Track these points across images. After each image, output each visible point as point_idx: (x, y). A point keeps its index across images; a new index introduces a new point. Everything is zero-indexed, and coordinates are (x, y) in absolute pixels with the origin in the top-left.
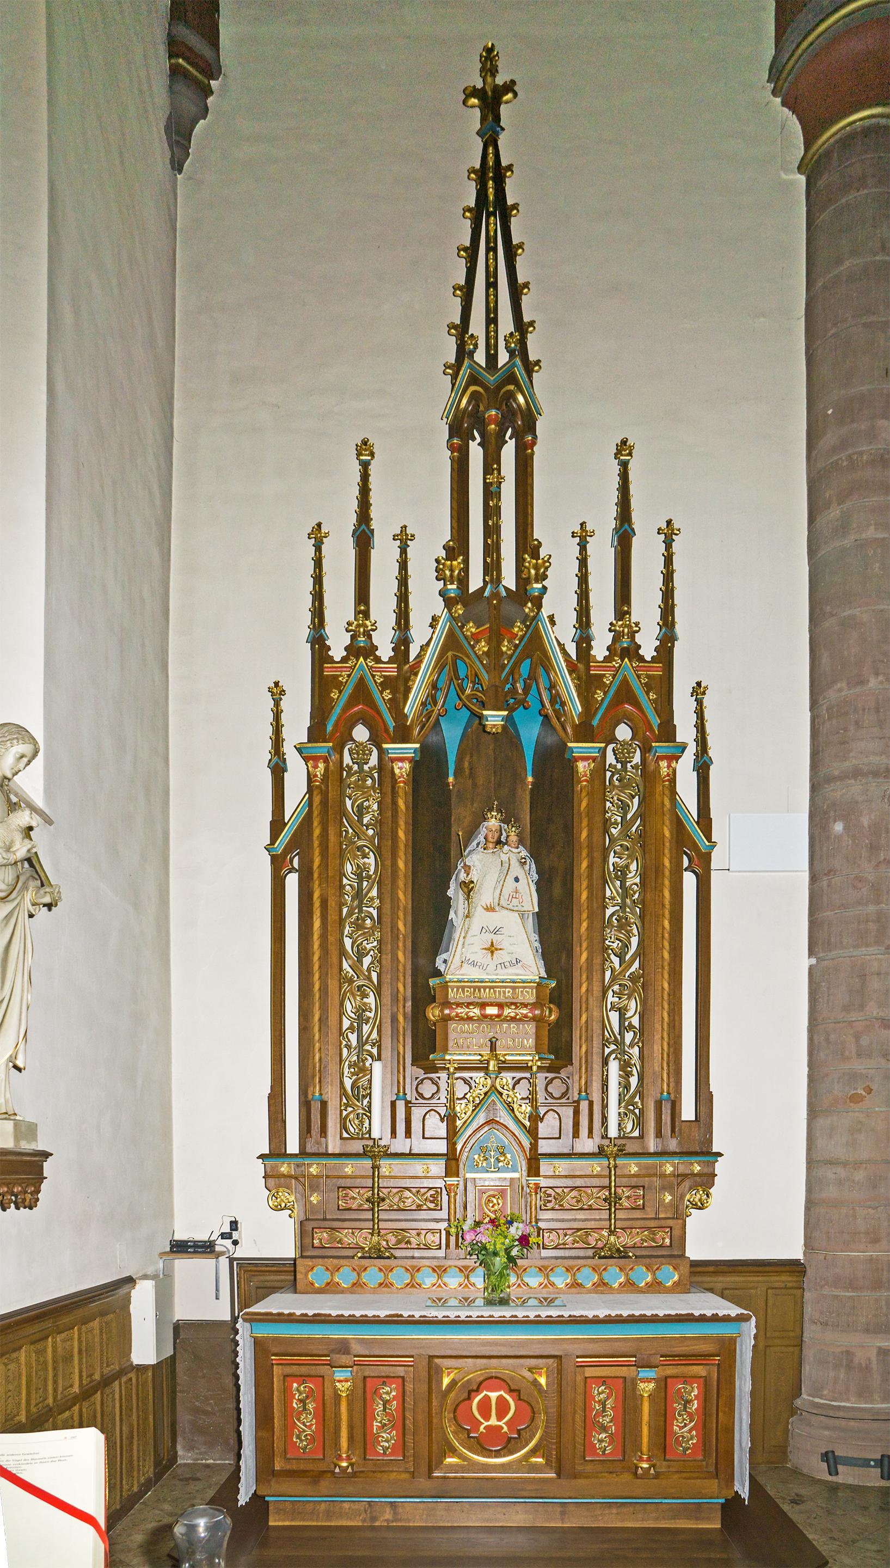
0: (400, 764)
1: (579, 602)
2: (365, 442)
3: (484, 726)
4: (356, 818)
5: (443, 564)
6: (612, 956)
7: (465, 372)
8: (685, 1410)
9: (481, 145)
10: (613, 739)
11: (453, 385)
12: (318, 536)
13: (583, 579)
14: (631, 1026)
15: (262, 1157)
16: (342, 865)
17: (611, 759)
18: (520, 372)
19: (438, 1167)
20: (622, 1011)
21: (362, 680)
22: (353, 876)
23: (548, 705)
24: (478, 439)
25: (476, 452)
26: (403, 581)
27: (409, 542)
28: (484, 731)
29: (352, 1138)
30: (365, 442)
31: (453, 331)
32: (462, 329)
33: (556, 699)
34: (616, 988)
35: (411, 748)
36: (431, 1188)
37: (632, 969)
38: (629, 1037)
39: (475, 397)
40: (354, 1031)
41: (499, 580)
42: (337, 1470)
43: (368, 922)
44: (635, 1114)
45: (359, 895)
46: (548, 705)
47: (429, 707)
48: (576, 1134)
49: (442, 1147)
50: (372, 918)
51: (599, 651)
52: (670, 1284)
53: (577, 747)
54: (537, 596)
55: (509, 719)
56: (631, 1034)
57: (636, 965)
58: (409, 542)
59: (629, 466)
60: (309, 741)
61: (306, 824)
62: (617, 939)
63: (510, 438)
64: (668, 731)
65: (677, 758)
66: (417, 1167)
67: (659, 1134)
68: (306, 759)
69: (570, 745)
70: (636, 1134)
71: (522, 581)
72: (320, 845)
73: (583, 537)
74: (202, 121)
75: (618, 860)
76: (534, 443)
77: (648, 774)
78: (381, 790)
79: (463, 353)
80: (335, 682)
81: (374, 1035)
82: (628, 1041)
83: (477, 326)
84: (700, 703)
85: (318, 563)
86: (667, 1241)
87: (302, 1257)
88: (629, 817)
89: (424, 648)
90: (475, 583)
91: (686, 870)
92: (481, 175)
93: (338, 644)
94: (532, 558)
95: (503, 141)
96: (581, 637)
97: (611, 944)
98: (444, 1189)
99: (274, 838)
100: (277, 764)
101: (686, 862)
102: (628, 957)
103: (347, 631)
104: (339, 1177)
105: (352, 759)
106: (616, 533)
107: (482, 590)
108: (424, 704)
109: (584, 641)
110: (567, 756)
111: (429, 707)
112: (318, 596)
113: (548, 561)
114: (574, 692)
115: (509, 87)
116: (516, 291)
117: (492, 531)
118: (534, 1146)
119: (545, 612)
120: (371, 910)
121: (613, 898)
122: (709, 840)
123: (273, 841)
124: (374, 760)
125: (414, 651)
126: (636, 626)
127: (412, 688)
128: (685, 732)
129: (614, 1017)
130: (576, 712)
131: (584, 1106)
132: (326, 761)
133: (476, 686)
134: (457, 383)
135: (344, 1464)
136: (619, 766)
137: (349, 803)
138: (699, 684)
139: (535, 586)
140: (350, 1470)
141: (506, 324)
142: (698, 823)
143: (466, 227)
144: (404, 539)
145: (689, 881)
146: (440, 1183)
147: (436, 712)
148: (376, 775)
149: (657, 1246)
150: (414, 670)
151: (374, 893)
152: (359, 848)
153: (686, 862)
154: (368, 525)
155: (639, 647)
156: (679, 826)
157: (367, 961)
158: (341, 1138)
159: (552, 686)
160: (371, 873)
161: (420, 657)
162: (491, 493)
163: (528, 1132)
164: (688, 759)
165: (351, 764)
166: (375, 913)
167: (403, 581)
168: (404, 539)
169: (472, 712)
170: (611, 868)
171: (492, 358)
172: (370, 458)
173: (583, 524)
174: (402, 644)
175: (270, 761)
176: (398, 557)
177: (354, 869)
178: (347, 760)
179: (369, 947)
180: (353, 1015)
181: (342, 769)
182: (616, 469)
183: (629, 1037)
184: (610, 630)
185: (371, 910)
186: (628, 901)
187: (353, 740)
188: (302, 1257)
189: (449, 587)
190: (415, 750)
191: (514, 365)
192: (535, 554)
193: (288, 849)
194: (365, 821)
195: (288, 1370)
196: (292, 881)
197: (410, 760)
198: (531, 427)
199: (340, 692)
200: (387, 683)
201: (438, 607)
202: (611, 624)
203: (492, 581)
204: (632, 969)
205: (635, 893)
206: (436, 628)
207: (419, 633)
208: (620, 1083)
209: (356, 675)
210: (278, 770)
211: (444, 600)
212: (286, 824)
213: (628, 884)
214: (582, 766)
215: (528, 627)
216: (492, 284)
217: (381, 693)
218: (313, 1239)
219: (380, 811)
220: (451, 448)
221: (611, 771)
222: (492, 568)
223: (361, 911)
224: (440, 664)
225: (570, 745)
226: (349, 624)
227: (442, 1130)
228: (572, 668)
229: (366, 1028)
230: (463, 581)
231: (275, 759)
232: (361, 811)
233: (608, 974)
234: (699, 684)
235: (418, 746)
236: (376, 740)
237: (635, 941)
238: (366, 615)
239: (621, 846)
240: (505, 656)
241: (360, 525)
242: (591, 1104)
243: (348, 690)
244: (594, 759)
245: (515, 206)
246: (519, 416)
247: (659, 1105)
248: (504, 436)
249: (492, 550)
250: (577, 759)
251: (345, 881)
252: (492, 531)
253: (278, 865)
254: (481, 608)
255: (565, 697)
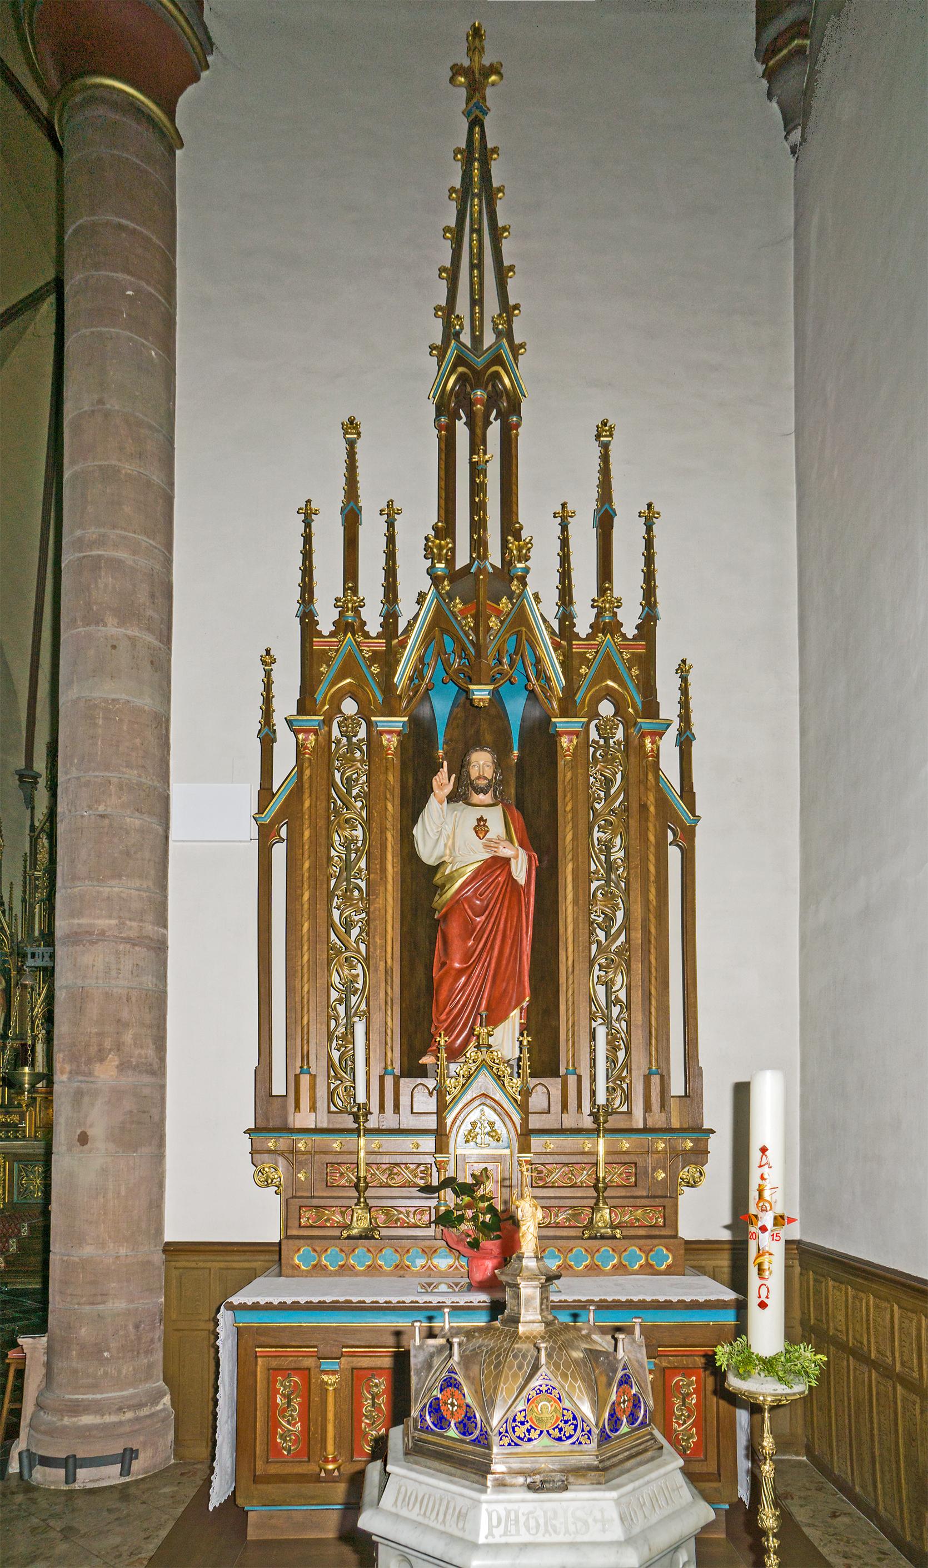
0: (388, 737)
1: (562, 581)
2: (351, 421)
3: (472, 700)
4: (345, 790)
5: (433, 542)
6: (598, 931)
7: (451, 353)
8: (684, 1404)
9: (466, 126)
10: (596, 715)
11: (440, 367)
12: (308, 515)
13: (565, 558)
14: (618, 1000)
15: (248, 1131)
16: (329, 837)
17: (594, 735)
18: (506, 353)
19: (428, 1143)
20: (608, 985)
21: (350, 655)
22: (342, 848)
23: (532, 678)
24: (464, 419)
25: (462, 432)
26: (391, 555)
27: (396, 516)
28: (473, 706)
29: (341, 1112)
30: (351, 421)
31: (448, 235)
32: (448, 312)
33: (541, 674)
34: (603, 961)
35: (398, 722)
36: (419, 1164)
37: (618, 943)
38: (616, 1011)
39: (462, 379)
40: (342, 1002)
41: (485, 557)
42: (323, 1474)
43: (356, 893)
44: (622, 1089)
45: (348, 866)
46: (532, 678)
47: (416, 681)
48: (565, 1107)
49: (431, 1123)
50: (360, 889)
51: (582, 627)
52: (664, 1267)
53: (560, 723)
54: (521, 576)
55: (495, 693)
56: (618, 1007)
57: (622, 938)
58: (396, 516)
59: (610, 448)
60: (299, 713)
61: (296, 793)
62: (603, 913)
63: (495, 419)
64: (651, 709)
65: (661, 735)
66: (407, 1143)
67: (647, 1108)
68: (296, 732)
69: (553, 720)
70: (624, 1109)
71: (507, 563)
72: (56, 495)
73: (564, 518)
74: (191, 89)
75: (601, 834)
76: (518, 426)
77: (631, 748)
78: (369, 762)
79: (450, 334)
80: (324, 657)
81: (363, 1007)
82: (615, 1015)
83: (463, 307)
84: (684, 679)
85: (308, 539)
86: (661, 1221)
87: (288, 1237)
88: (612, 791)
89: (411, 625)
90: (462, 560)
91: (671, 844)
92: (467, 155)
93: (326, 619)
94: (516, 540)
95: (489, 122)
96: (564, 614)
97: (596, 918)
98: (433, 1165)
99: (261, 809)
100: (267, 735)
101: (670, 837)
102: (613, 931)
103: (336, 606)
104: (325, 1153)
105: (341, 732)
106: (597, 514)
107: (469, 567)
108: (411, 679)
109: (566, 618)
110: (551, 731)
111: (416, 681)
112: (307, 571)
113: (530, 542)
114: (559, 669)
115: (494, 69)
116: (502, 274)
117: (477, 508)
118: (525, 1121)
119: (530, 591)
120: (359, 881)
121: (597, 872)
122: (694, 815)
123: (260, 810)
124: (362, 733)
125: (402, 624)
126: (618, 602)
127: (400, 661)
128: (669, 709)
129: (601, 991)
130: (559, 685)
131: (572, 1080)
132: (316, 733)
133: (463, 661)
134: (443, 367)
135: (331, 1467)
136: (602, 742)
137: (337, 776)
138: (684, 661)
139: (519, 565)
140: (336, 1473)
141: (492, 306)
142: (681, 797)
143: (453, 208)
144: (390, 514)
145: (674, 855)
146: (430, 1159)
147: (424, 686)
148: (364, 747)
149: (650, 1226)
150: (403, 644)
151: (363, 864)
152: (347, 821)
153: (670, 837)
154: (357, 502)
155: (621, 625)
156: (663, 801)
157: (355, 932)
158: (329, 1112)
159: (538, 661)
160: (359, 845)
161: (407, 631)
162: (476, 470)
163: (519, 1106)
164: (671, 734)
165: (340, 736)
166: (363, 885)
167: (391, 555)
168: (390, 514)
169: (460, 688)
170: (596, 842)
171: (477, 339)
172: (355, 436)
173: (564, 505)
174: (390, 618)
175: (260, 731)
176: (385, 531)
177: (343, 841)
178: (336, 732)
179: (356, 918)
180: (341, 987)
181: (330, 741)
182: (597, 451)
183: (616, 1011)
184: (593, 606)
185: (359, 881)
186: (613, 877)
187: (341, 712)
188: (288, 1237)
189: (438, 565)
190: (404, 722)
191: (500, 347)
192: (518, 537)
193: (277, 819)
194: (354, 793)
195: (274, 1363)
196: (279, 852)
197: (399, 733)
198: (515, 408)
199: (329, 666)
200: (375, 657)
201: (425, 584)
202: (593, 600)
203: (478, 556)
204: (618, 943)
205: (619, 867)
206: (422, 605)
207: (406, 608)
208: (607, 1057)
209: (344, 650)
210: (267, 741)
211: (431, 578)
212: (274, 795)
213: (612, 858)
214: (564, 741)
215: (513, 604)
216: (477, 265)
217: (370, 667)
218: (300, 1218)
219: (369, 784)
220: (439, 427)
221: (593, 747)
222: (478, 545)
223: (348, 880)
224: (428, 639)
225: (553, 720)
226: (337, 600)
227: (431, 1105)
228: (557, 647)
229: (354, 999)
230: (450, 562)
231: (266, 730)
232: (349, 783)
233: (594, 947)
234: (684, 661)
235: (406, 719)
236: (365, 713)
237: (620, 915)
238: (355, 591)
239: (605, 820)
240: (492, 632)
241: (348, 502)
242: (579, 1078)
243: (337, 664)
244: (577, 734)
245: (500, 190)
246: (504, 398)
247: (647, 1079)
248: (489, 416)
249: (478, 526)
250: (560, 734)
251: (333, 853)
252: (477, 508)
253: (266, 837)
254: (466, 583)
255: (550, 673)
